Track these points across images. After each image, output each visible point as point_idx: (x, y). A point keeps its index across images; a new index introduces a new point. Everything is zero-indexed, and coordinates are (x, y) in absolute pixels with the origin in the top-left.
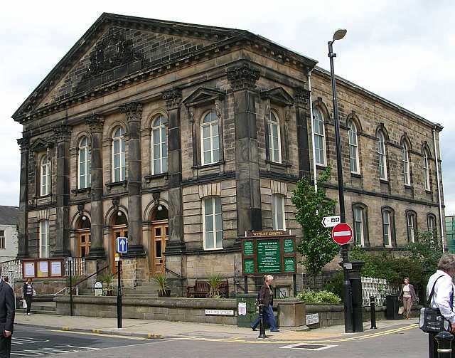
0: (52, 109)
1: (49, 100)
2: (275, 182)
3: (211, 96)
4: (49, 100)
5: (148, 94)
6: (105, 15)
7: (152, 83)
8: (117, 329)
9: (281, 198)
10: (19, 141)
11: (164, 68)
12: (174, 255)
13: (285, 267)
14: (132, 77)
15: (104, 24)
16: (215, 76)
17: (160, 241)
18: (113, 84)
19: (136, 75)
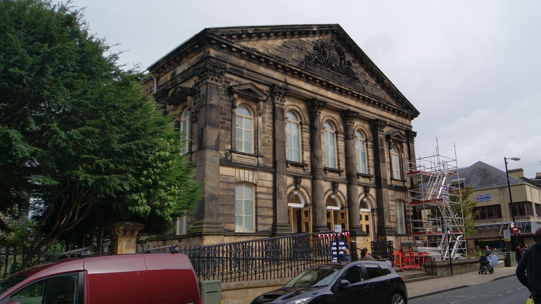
0: (242, 53)
1: (250, 45)
2: (399, 193)
3: (403, 139)
4: (250, 45)
5: (302, 91)
6: (338, 26)
7: (370, 109)
8: (205, 292)
9: (401, 202)
10: (415, 134)
11: (379, 104)
12: (392, 236)
13: (381, 236)
14: (360, 94)
15: (333, 31)
16: (400, 127)
17: (342, 218)
18: (346, 89)
19: (358, 93)
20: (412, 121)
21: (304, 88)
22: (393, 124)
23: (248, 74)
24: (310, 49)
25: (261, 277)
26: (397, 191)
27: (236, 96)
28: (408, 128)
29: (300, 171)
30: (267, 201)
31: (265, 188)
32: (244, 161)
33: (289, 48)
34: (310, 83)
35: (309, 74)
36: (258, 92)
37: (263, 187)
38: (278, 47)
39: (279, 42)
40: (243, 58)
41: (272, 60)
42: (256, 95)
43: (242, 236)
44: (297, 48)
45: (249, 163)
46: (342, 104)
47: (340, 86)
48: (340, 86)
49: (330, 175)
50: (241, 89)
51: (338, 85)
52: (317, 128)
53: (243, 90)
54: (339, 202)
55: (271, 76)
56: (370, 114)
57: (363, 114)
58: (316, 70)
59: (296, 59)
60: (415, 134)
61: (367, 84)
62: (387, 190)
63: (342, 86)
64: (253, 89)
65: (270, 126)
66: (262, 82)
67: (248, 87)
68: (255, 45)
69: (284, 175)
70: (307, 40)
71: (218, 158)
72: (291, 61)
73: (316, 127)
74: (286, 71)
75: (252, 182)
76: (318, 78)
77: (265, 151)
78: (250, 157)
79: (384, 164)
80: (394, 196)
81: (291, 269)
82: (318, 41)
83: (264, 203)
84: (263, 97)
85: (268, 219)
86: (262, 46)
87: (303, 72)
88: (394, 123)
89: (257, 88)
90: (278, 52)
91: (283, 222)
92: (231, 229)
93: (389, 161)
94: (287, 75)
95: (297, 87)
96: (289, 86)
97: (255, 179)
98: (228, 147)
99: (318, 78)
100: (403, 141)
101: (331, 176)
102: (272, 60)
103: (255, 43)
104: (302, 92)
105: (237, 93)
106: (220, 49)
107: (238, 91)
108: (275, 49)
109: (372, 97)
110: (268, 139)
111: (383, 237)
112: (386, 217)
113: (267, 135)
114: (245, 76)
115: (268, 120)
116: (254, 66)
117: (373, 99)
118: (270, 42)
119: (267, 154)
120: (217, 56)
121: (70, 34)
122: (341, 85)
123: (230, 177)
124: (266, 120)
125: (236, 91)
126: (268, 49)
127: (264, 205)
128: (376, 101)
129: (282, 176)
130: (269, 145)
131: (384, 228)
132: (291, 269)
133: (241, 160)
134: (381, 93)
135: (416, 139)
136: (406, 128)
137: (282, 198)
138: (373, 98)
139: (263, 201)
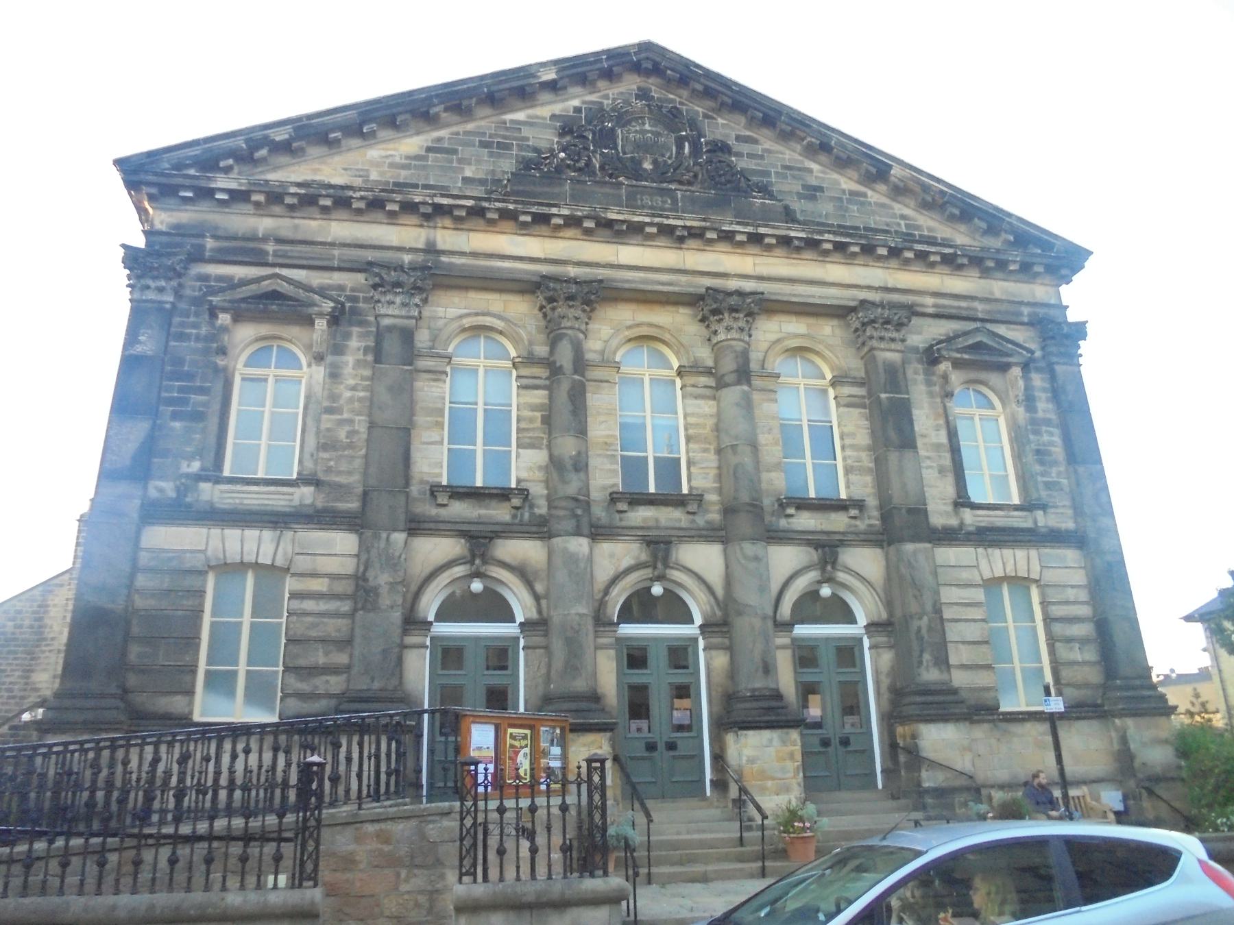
10: (1080, 331)
20: (1064, 289)
21: (508, 253)
22: (959, 308)
23: (279, 253)
24: (547, 138)
25: (91, 882)
26: (990, 546)
27: (224, 318)
28: (1036, 314)
29: (838, 522)
30: (325, 620)
31: (321, 580)
32: (245, 502)
33: (455, 152)
34: (534, 236)
35: (511, 207)
36: (302, 294)
37: (314, 575)
38: (408, 157)
39: (411, 144)
40: (265, 213)
41: (358, 195)
42: (293, 306)
43: (1023, 720)
44: (484, 145)
45: (263, 508)
46: (683, 279)
47: (657, 220)
48: (657, 220)
49: (806, 521)
50: (239, 296)
51: (647, 220)
52: (561, 367)
53: (244, 300)
54: (861, 609)
55: (377, 243)
56: (833, 291)
57: (795, 295)
58: (557, 190)
59: (477, 177)
60: (1080, 331)
61: (813, 198)
62: (928, 545)
63: (667, 217)
64: (285, 288)
65: (360, 388)
66: (336, 263)
67: (266, 285)
68: (319, 170)
69: (395, 530)
70: (529, 117)
71: (137, 502)
72: (460, 185)
73: (558, 364)
74: (681, 239)
75: (1013, 574)
76: (554, 210)
77: (332, 463)
78: (272, 489)
79: (909, 454)
80: (977, 567)
81: (102, 864)
82: (577, 110)
83: (313, 626)
84: (321, 306)
85: (328, 678)
86: (345, 169)
87: (486, 204)
88: (963, 304)
89: (289, 281)
90: (404, 173)
91: (376, 685)
92: (173, 710)
93: (943, 438)
94: (435, 227)
95: (474, 255)
96: (444, 259)
97: (285, 554)
98: (188, 466)
99: (554, 210)
100: (1011, 360)
101: (645, 520)
102: (358, 195)
103: (317, 166)
104: (499, 269)
105: (224, 310)
106: (183, 207)
107: (226, 305)
108: (392, 165)
109: (821, 233)
110: (347, 428)
111: (906, 728)
112: (922, 652)
113: (346, 416)
114: (271, 259)
115: (354, 372)
116: (312, 226)
117: (827, 236)
118: (374, 153)
119: (339, 473)
120: (177, 227)
121: (833, 336)
122: (660, 216)
123: (188, 555)
124: (348, 370)
125: (221, 304)
126: (367, 170)
127: (313, 633)
128: (848, 240)
129: (384, 535)
130: (351, 446)
131: (1154, 687)
132: (102, 864)
133: (237, 501)
134: (905, 213)
135: (1085, 347)
136: (1029, 315)
137: (379, 608)
138: (829, 232)
139: (309, 619)
